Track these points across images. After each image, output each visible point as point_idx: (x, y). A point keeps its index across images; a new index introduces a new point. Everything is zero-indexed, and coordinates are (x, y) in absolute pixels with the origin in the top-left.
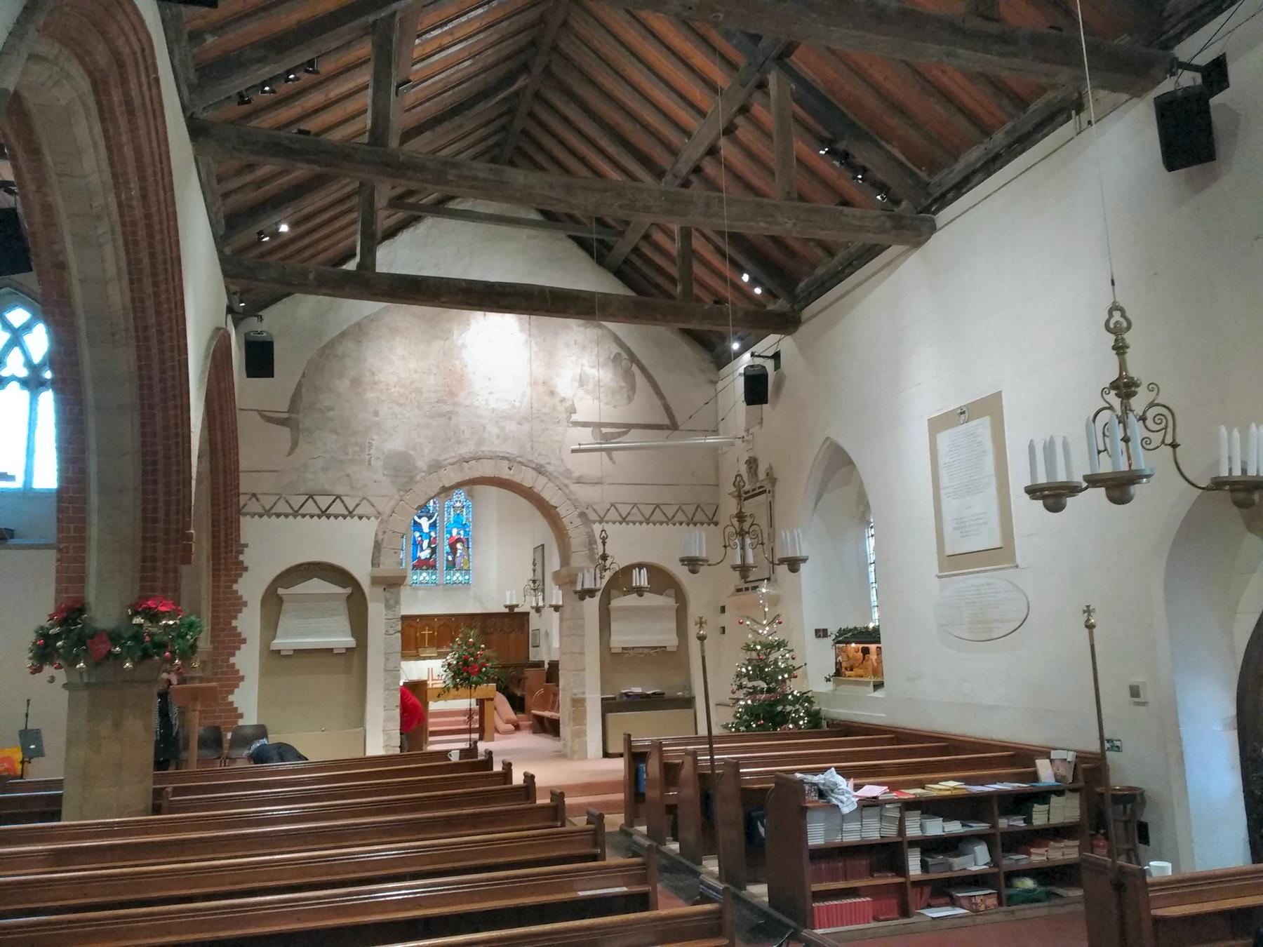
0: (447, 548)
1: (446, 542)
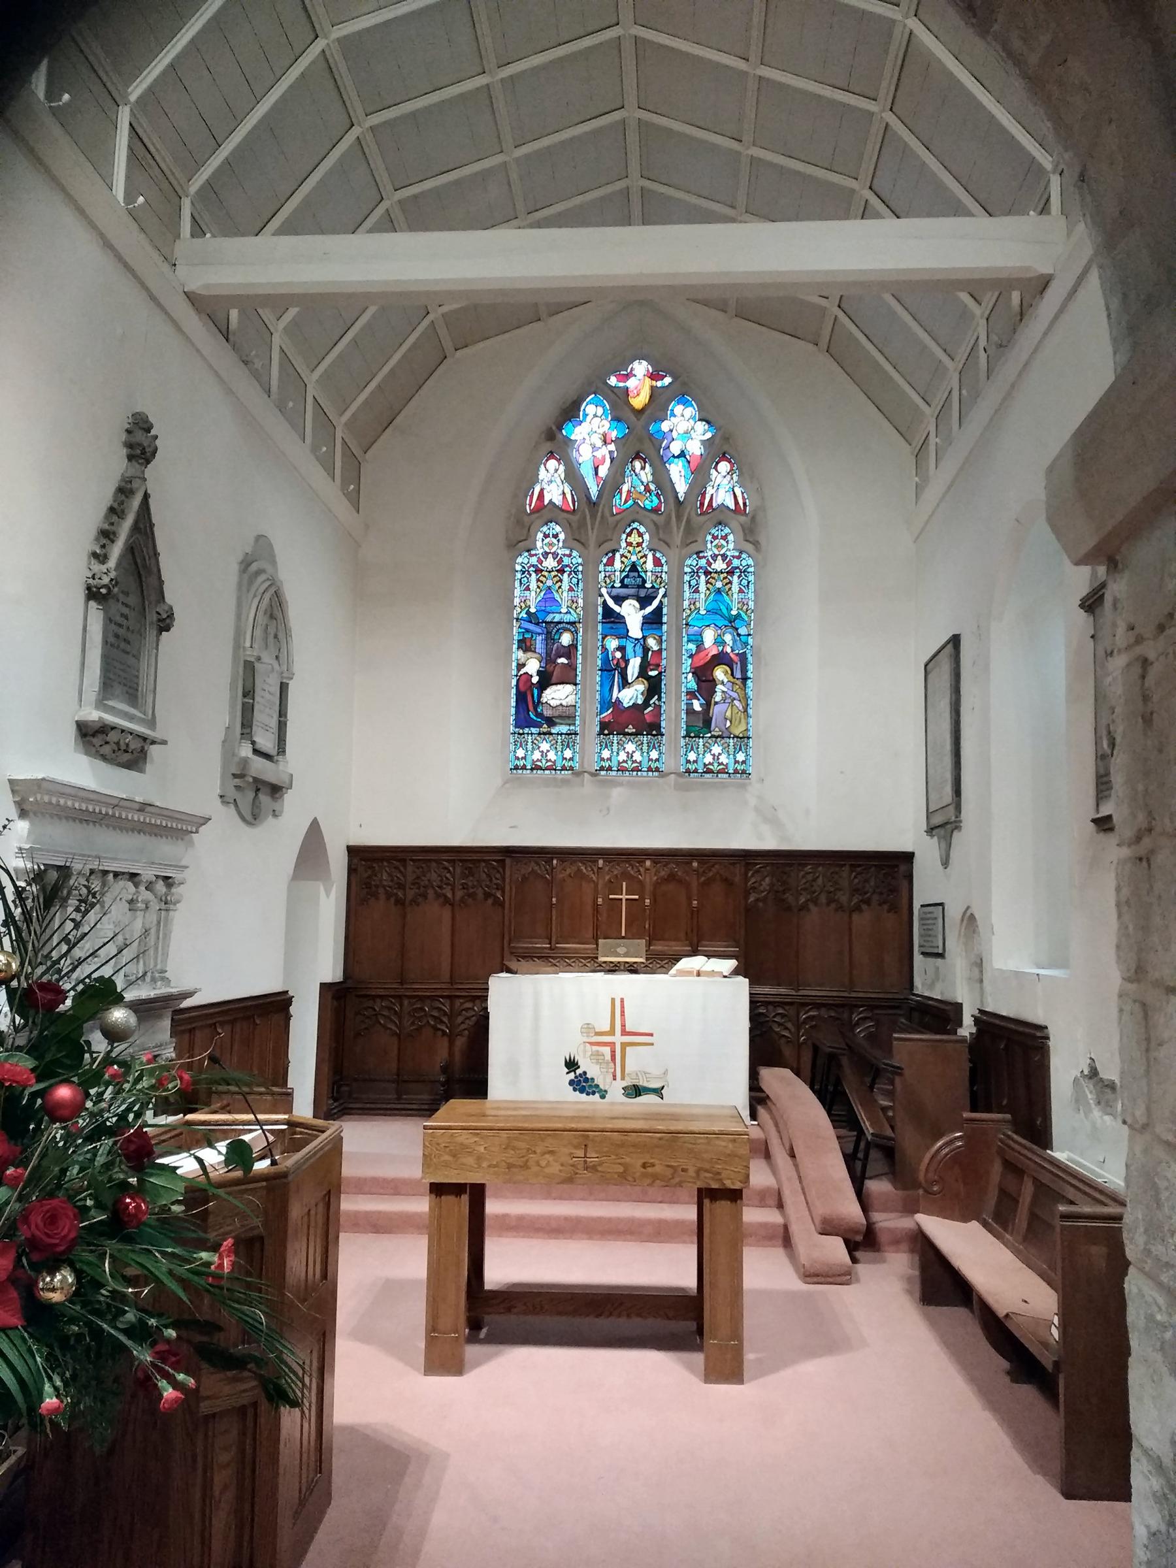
0: (691, 683)
1: (687, 664)
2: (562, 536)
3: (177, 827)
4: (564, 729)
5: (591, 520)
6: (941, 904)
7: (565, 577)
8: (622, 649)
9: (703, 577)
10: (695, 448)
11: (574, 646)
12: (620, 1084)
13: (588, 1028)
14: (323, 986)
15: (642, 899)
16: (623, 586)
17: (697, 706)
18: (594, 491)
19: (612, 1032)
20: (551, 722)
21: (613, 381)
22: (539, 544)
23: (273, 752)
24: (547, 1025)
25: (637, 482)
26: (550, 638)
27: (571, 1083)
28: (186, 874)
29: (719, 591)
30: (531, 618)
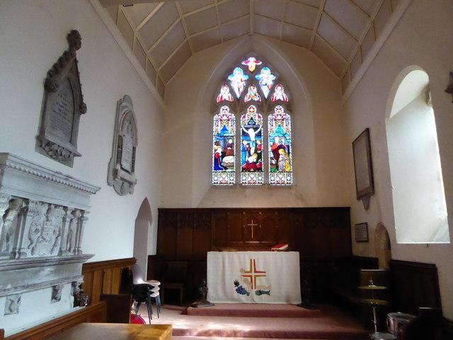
0: (271, 155)
1: (270, 149)
2: (228, 110)
3: (86, 190)
4: (230, 170)
5: (238, 106)
6: (366, 223)
7: (230, 122)
8: (248, 144)
9: (274, 121)
10: (270, 83)
11: (233, 144)
12: (254, 290)
13: (242, 270)
14: (149, 256)
15: (259, 225)
16: (249, 124)
17: (274, 162)
18: (238, 96)
19: (251, 272)
20: (226, 168)
21: (243, 63)
22: (221, 112)
23: (130, 171)
24: (224, 268)
25: (252, 93)
26: (225, 141)
27: (237, 290)
28: (90, 210)
29: (279, 126)
30: (218, 135)
